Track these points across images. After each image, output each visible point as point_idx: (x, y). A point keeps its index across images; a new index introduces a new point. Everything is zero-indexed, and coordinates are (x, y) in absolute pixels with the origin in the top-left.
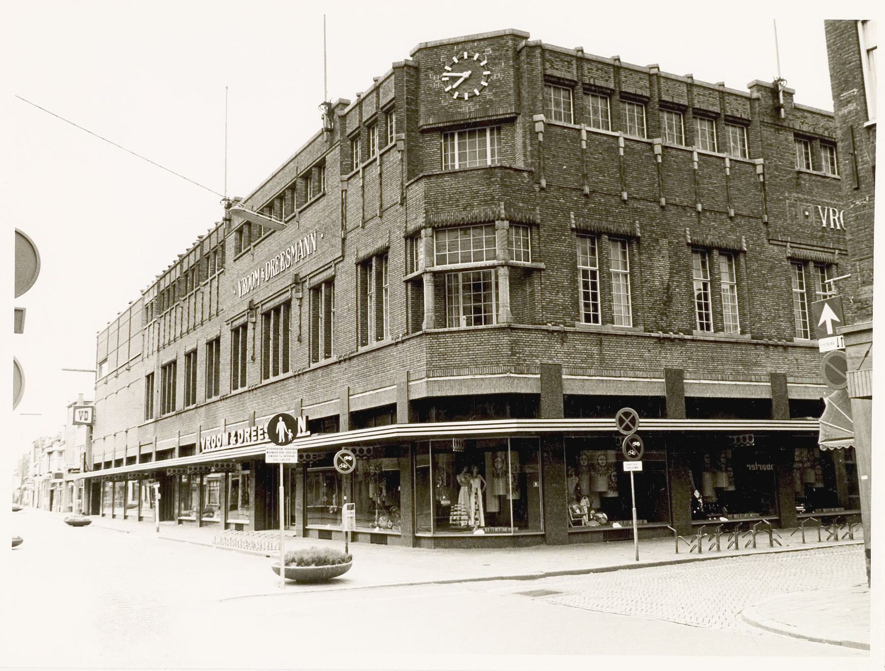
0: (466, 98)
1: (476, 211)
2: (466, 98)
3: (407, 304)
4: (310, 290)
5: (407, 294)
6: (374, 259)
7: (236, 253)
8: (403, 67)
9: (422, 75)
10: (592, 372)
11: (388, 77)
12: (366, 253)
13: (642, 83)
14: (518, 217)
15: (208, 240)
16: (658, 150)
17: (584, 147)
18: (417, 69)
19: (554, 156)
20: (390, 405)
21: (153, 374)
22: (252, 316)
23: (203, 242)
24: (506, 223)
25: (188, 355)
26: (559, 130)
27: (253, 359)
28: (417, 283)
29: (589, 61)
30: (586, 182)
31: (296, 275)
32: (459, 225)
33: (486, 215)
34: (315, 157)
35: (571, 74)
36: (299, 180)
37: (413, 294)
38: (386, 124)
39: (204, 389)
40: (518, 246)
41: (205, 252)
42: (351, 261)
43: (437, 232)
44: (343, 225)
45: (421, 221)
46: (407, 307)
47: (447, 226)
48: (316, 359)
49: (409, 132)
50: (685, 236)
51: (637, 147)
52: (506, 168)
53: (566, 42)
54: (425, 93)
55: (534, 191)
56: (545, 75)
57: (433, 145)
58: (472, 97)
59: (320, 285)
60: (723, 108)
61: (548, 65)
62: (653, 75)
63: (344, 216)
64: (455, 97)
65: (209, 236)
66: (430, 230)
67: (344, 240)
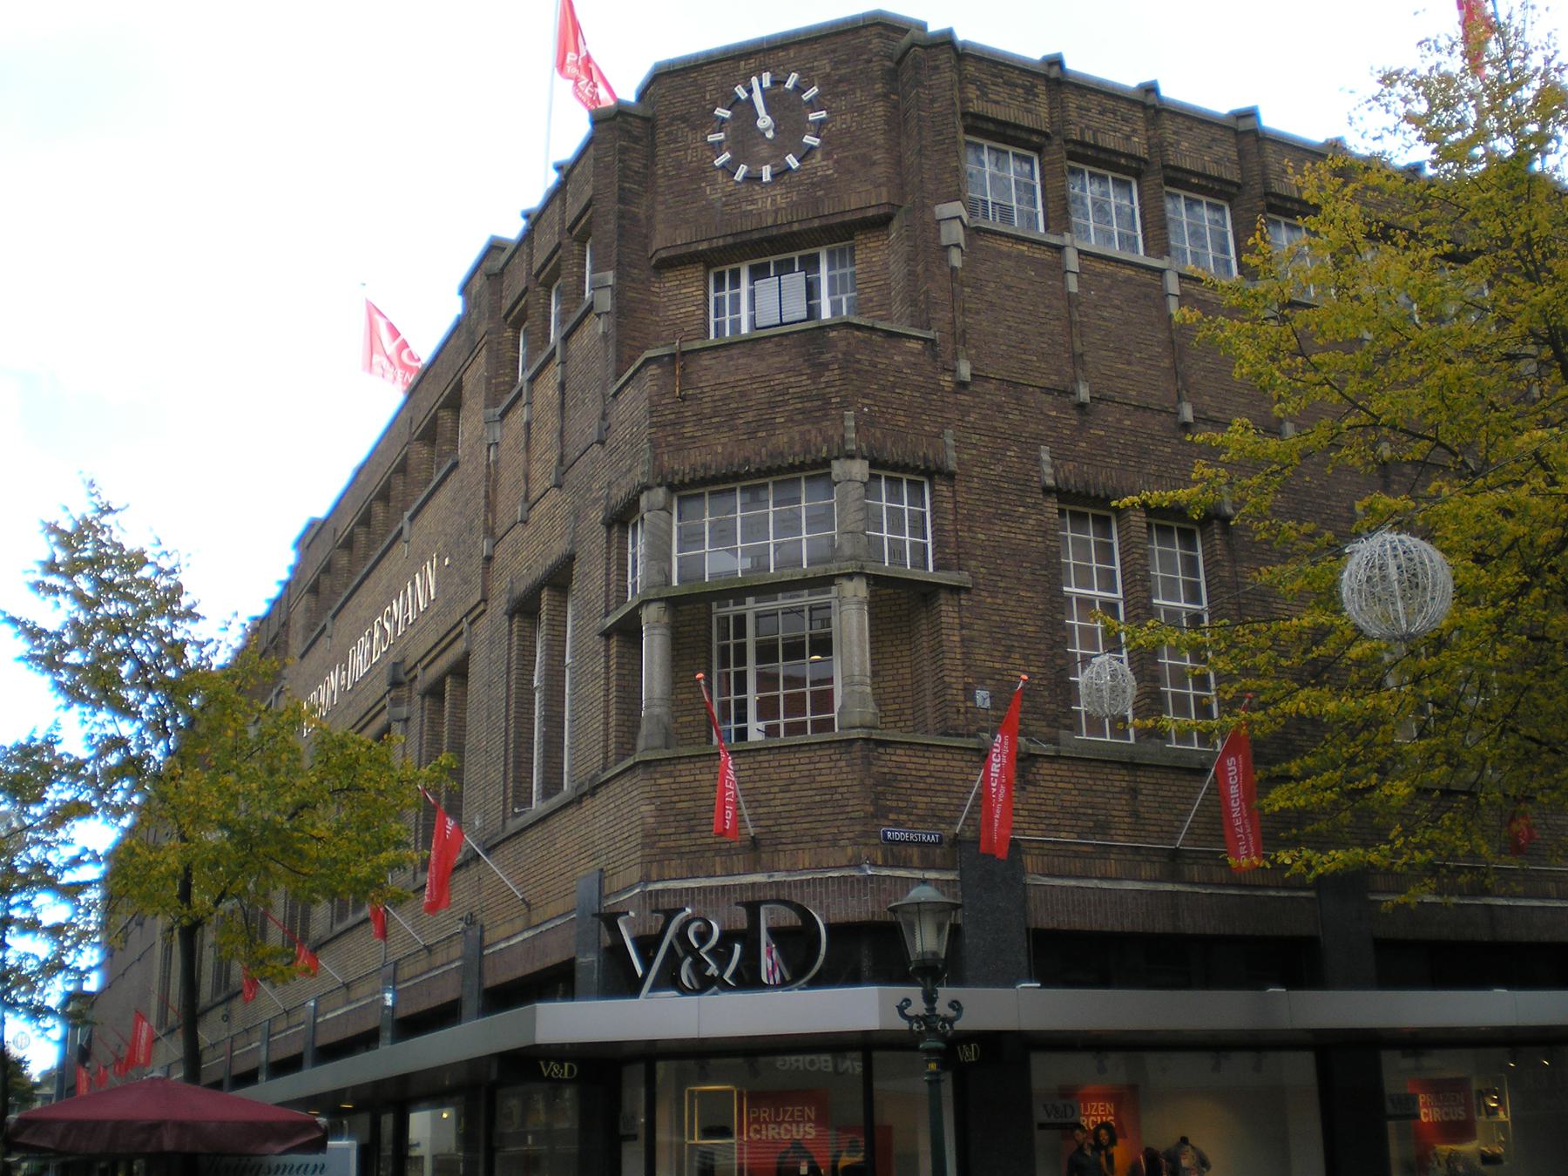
0: (767, 177)
1: (781, 439)
8: (613, 118)
9: (661, 136)
10: (1113, 867)
13: (1218, 150)
14: (893, 452)
20: (564, 963)
24: (860, 469)
26: (1005, 246)
28: (628, 632)
35: (1038, 115)
36: (417, 446)
37: (620, 666)
40: (896, 527)
42: (499, 606)
45: (639, 475)
47: (704, 482)
53: (1024, 42)
54: (665, 175)
56: (965, 115)
57: (680, 293)
58: (781, 173)
59: (440, 681)
61: (972, 91)
63: (490, 505)
64: (739, 176)
66: (659, 494)
67: (489, 559)
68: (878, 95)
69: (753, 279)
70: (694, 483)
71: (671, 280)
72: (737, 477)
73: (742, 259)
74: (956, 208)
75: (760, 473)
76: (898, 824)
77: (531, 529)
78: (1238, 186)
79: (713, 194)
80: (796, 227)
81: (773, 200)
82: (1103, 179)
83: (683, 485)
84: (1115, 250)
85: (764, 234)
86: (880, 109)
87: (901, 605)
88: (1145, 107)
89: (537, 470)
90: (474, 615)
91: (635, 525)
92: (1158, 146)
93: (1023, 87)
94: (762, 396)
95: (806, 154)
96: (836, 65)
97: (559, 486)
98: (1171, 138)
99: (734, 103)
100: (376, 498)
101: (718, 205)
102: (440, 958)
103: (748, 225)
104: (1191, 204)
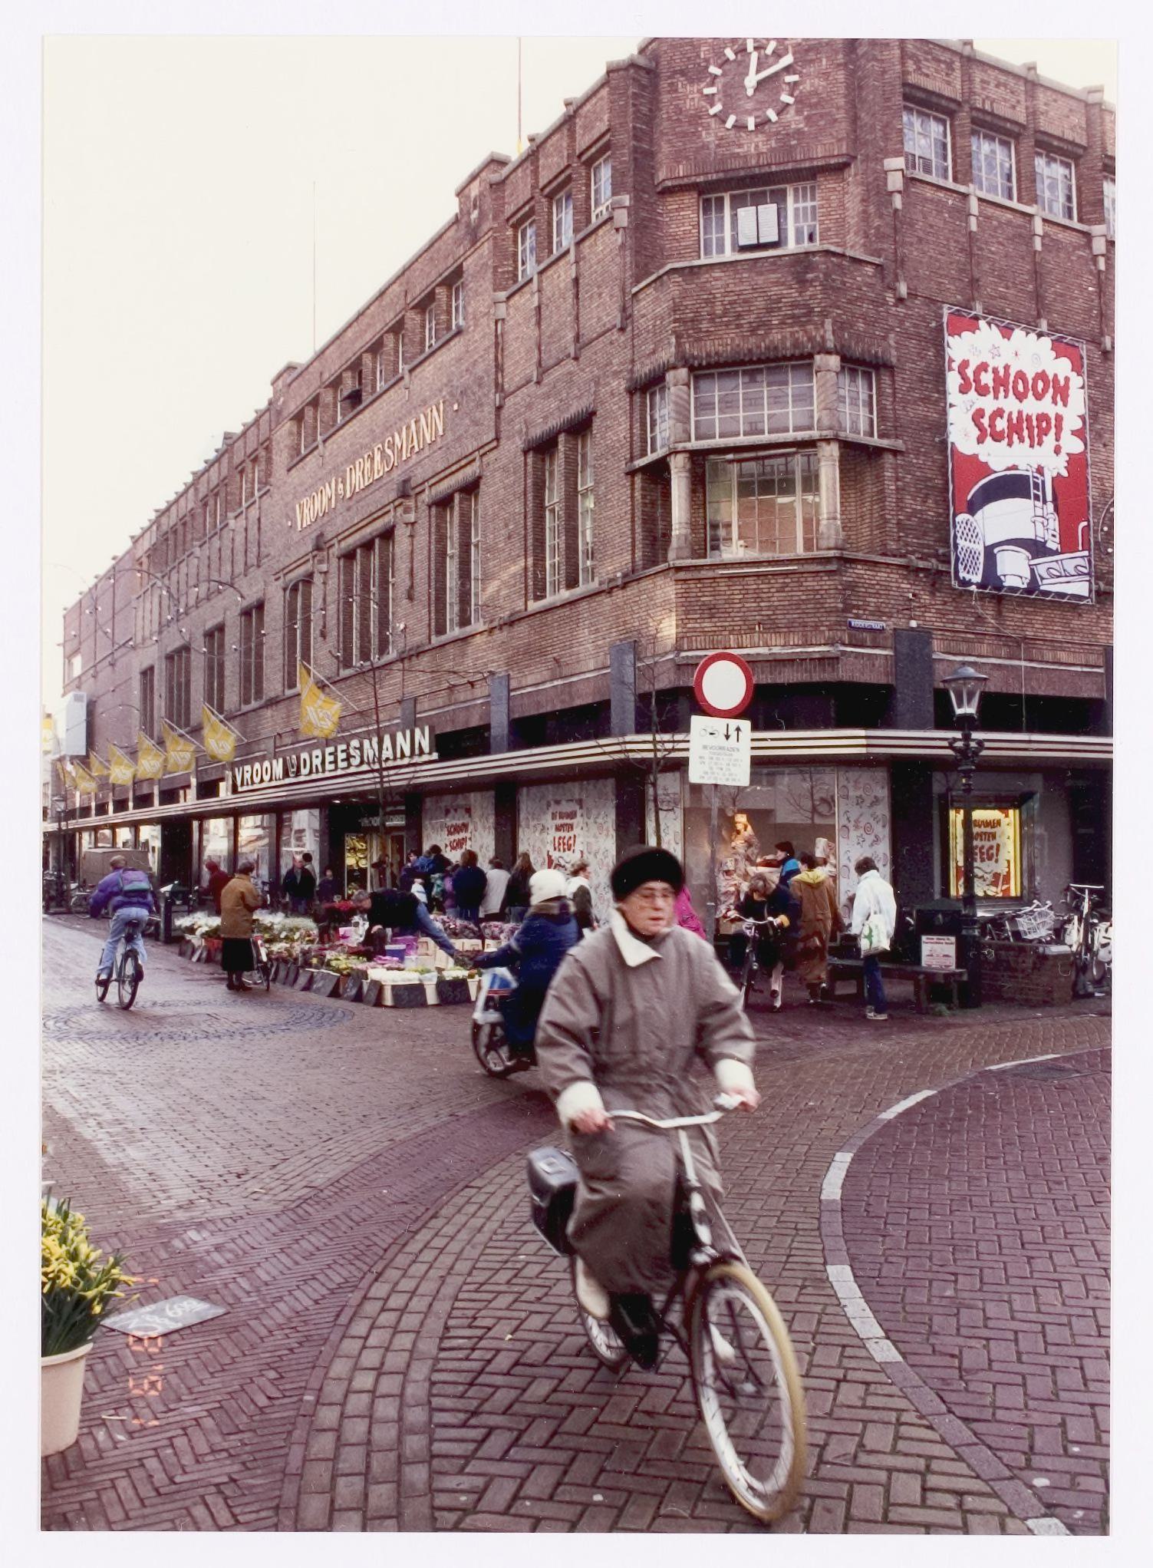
0: (751, 127)
1: (776, 336)
2: (751, 127)
3: (633, 517)
4: (430, 507)
5: (632, 497)
6: (562, 438)
7: (292, 457)
9: (664, 85)
10: (985, 649)
11: (594, 93)
12: (546, 428)
14: (857, 350)
15: (240, 443)
17: (974, 227)
18: (652, 73)
19: (920, 240)
21: (151, 668)
22: (321, 562)
23: (232, 445)
24: (834, 361)
25: (209, 635)
26: (929, 193)
27: (323, 635)
28: (657, 474)
29: (985, 65)
30: (976, 295)
31: (406, 482)
32: (742, 363)
33: (796, 344)
34: (445, 267)
36: (411, 314)
37: (644, 497)
38: (588, 186)
39: (236, 689)
41: (236, 461)
42: (512, 447)
43: (697, 378)
44: (497, 384)
45: (667, 354)
46: (633, 521)
47: (717, 365)
48: (441, 630)
49: (637, 193)
51: (1061, 235)
52: (834, 254)
54: (669, 119)
55: (885, 303)
56: (905, 84)
57: (682, 217)
61: (911, 66)
63: (499, 368)
64: (729, 124)
65: (244, 433)
66: (683, 372)
67: (499, 408)
68: (839, 65)
69: (734, 207)
71: (672, 203)
72: (742, 363)
73: (726, 191)
74: (899, 162)
76: (858, 617)
77: (544, 389)
78: (1085, 148)
79: (709, 138)
80: (774, 168)
81: (757, 146)
82: (993, 139)
83: (701, 367)
85: (749, 172)
86: (841, 76)
87: (857, 457)
88: (1026, 81)
92: (1033, 114)
93: (945, 62)
94: (760, 303)
95: (782, 109)
97: (576, 359)
98: (1043, 108)
100: (366, 351)
101: (712, 146)
103: (736, 164)
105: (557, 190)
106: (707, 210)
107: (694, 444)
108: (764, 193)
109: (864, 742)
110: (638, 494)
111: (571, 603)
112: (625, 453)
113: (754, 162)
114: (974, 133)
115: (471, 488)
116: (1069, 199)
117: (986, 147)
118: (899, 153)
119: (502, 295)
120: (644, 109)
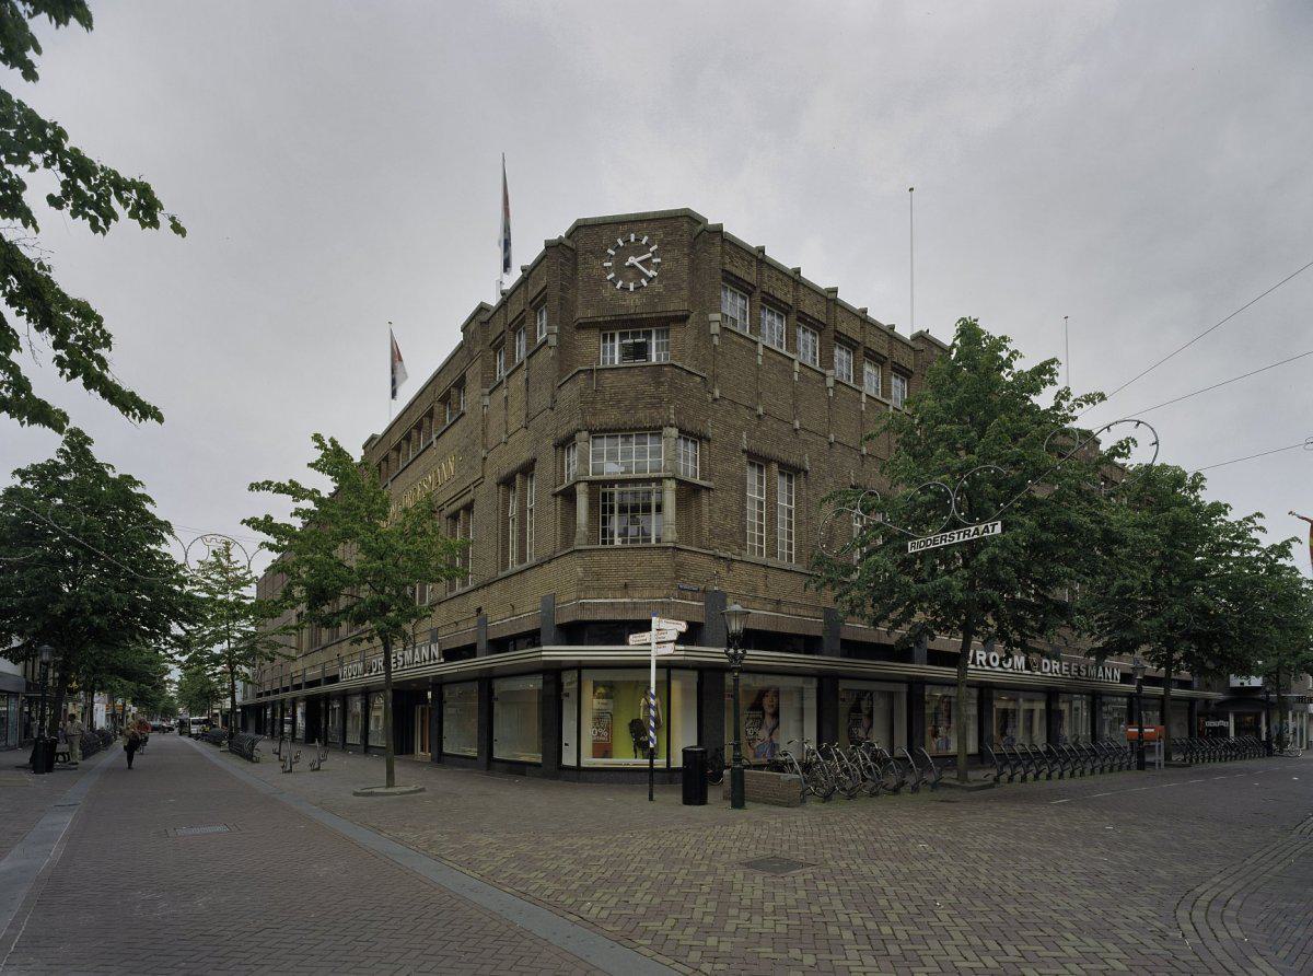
0: (632, 289)
1: (641, 415)
2: (632, 289)
6: (518, 476)
9: (580, 259)
14: (689, 427)
16: (830, 382)
24: (674, 432)
26: (735, 338)
28: (569, 495)
35: (751, 276)
37: (562, 509)
40: (686, 460)
47: (605, 431)
50: (849, 478)
51: (809, 374)
57: (589, 343)
60: (891, 354)
62: (831, 300)
64: (618, 286)
66: (585, 434)
67: (485, 459)
70: (601, 431)
72: (620, 430)
73: (617, 329)
74: (718, 316)
75: (631, 430)
79: (606, 294)
80: (644, 316)
84: (775, 347)
86: (686, 261)
87: (689, 492)
88: (794, 280)
89: (512, 419)
90: (477, 483)
91: (569, 448)
92: (796, 300)
94: (632, 394)
96: (666, 235)
99: (648, 245)
102: (462, 627)
104: (805, 331)
105: (517, 326)
106: (605, 340)
107: (591, 476)
108: (639, 332)
109: (683, 653)
110: (559, 508)
111: (521, 572)
112: (552, 483)
113: (632, 311)
114: (762, 308)
115: (468, 508)
116: (815, 354)
117: (769, 317)
118: (718, 310)
119: (487, 391)
120: (569, 274)
